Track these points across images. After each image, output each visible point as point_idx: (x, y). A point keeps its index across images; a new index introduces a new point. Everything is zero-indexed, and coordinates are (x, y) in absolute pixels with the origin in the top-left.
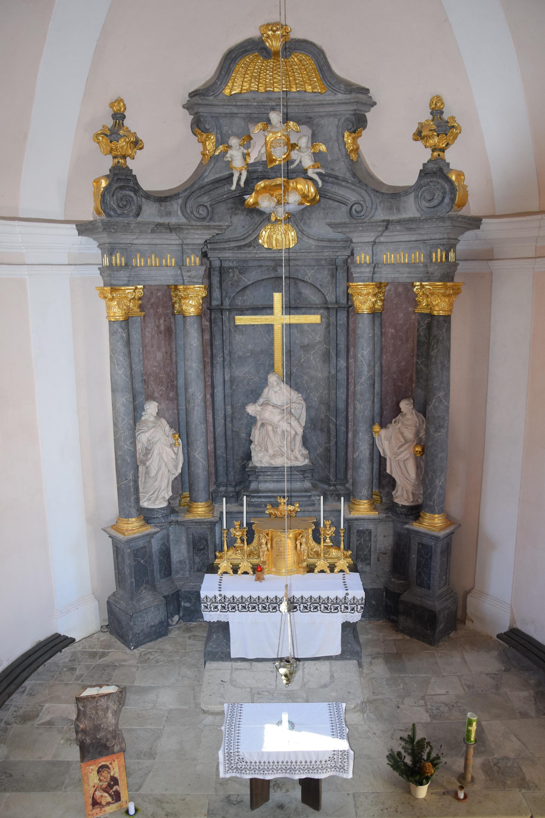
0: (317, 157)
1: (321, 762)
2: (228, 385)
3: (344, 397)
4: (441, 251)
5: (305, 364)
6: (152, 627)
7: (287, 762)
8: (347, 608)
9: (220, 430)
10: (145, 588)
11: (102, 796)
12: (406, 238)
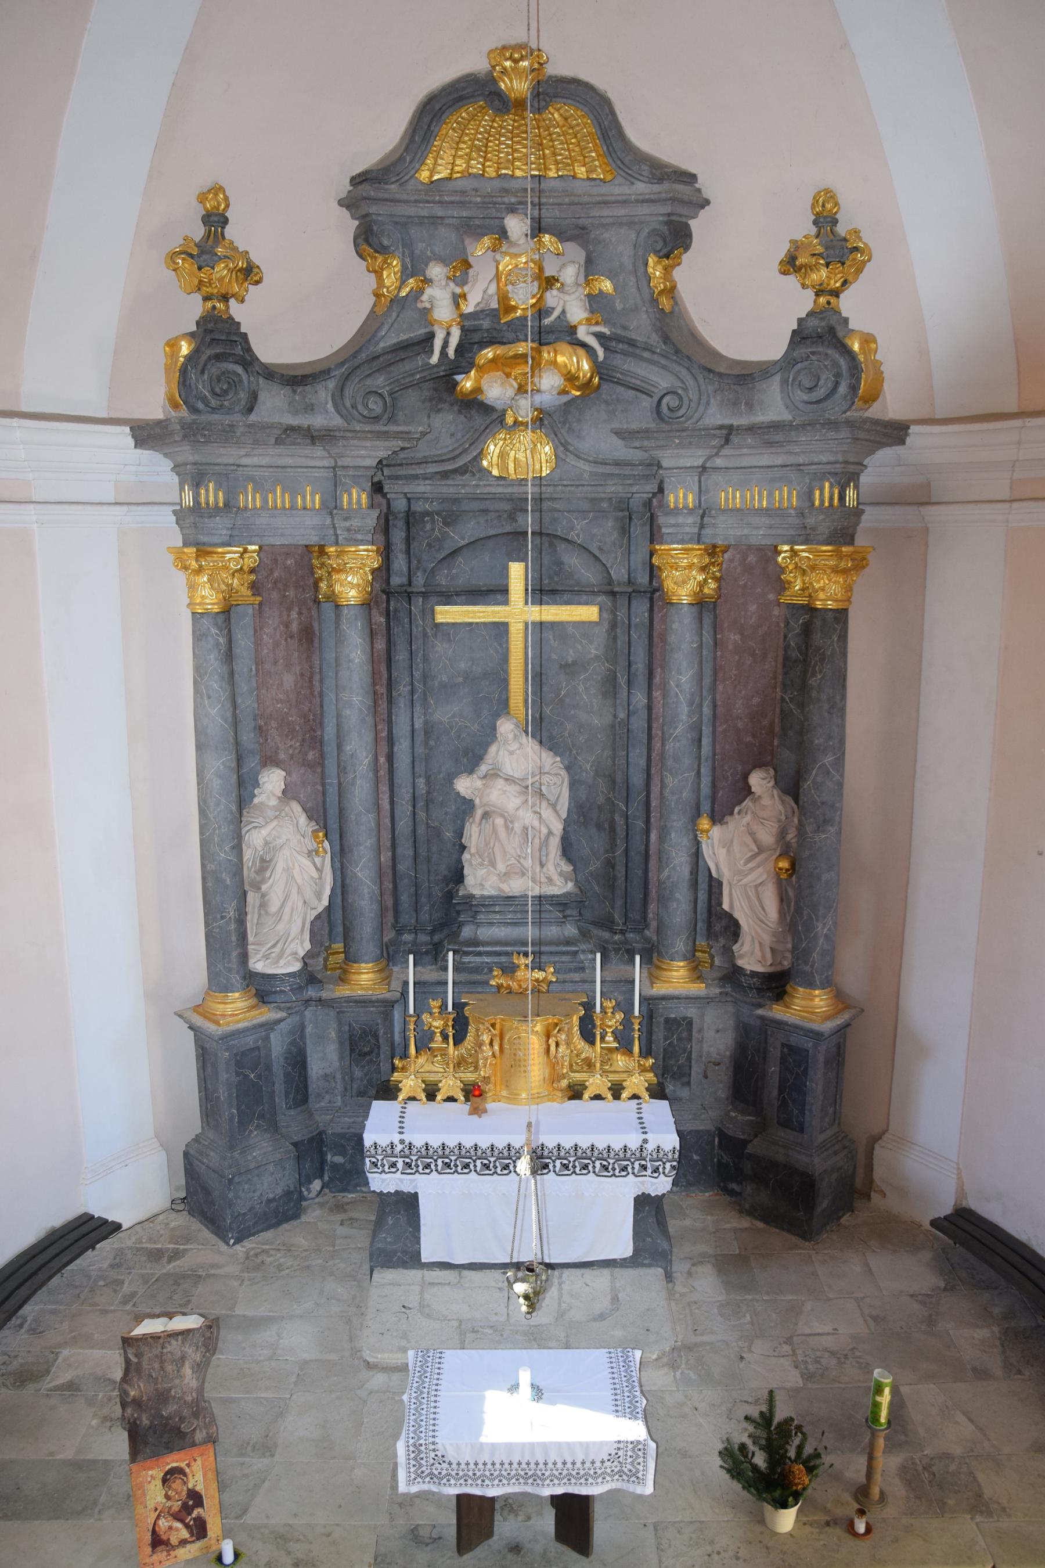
0: (595, 302)
1: (593, 1463)
2: (420, 738)
3: (643, 762)
4: (831, 487)
6: (269, 1201)
7: (528, 1464)
8: (644, 1168)
9: (403, 824)
10: (258, 1127)
11: (170, 1528)
12: (765, 460)
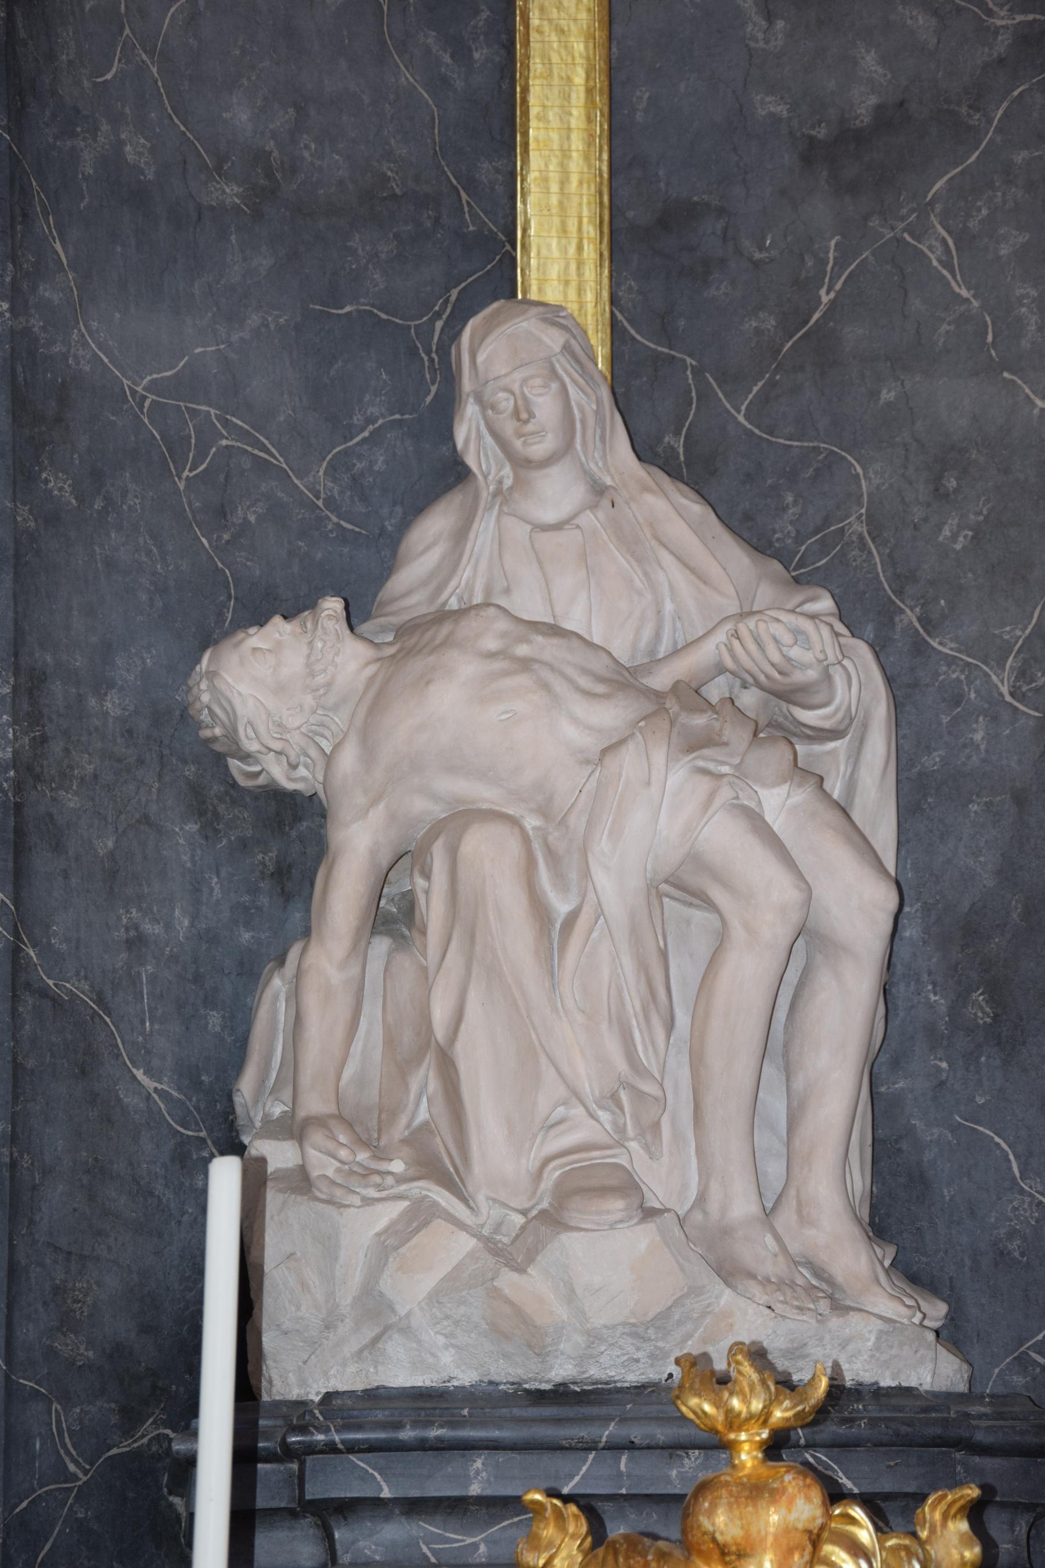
5: (854, 334)
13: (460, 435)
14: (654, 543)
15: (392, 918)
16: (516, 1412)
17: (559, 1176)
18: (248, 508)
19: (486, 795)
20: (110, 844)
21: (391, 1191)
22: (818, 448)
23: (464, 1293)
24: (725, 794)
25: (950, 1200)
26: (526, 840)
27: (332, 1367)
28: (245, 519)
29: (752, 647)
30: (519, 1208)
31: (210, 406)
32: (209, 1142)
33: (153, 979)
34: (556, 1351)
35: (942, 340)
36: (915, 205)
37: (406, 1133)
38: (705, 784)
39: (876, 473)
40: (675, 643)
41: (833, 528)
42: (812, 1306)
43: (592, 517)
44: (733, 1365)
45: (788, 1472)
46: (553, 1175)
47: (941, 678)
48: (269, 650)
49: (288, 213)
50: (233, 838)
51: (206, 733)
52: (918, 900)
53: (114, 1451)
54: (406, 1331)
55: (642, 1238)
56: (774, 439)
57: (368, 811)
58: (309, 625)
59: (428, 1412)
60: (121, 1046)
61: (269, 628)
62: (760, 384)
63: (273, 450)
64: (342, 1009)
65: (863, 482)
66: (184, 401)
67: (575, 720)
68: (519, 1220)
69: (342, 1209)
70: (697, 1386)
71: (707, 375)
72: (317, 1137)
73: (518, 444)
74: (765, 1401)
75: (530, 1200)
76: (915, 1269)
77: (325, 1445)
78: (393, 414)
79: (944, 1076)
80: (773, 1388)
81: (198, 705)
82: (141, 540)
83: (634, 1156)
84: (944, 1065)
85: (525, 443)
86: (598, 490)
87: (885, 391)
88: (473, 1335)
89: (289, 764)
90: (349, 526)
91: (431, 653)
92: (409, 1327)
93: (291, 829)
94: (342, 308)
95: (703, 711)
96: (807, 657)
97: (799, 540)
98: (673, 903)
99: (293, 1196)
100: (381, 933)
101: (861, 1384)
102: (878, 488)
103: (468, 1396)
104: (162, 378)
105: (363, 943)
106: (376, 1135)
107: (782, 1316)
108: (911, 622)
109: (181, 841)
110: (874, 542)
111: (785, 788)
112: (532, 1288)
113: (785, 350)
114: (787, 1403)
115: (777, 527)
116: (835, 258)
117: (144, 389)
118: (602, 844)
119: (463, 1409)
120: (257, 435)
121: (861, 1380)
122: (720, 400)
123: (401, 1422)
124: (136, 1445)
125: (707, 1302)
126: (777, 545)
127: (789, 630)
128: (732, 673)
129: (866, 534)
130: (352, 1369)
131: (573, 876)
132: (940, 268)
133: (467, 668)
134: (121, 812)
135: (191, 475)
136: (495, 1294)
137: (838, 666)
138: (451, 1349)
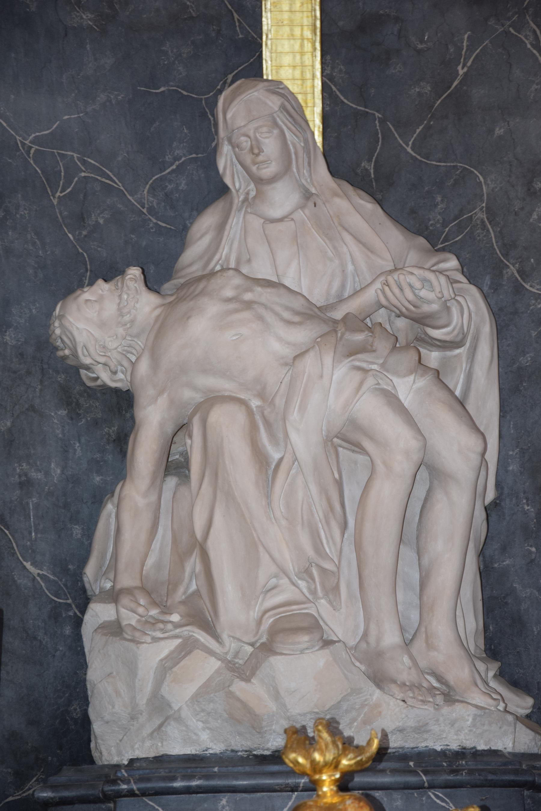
13: (221, 164)
14: (340, 228)
15: (174, 466)
16: (248, 769)
17: (272, 622)
18: (99, 215)
19: (226, 386)
20: (9, 424)
21: (170, 633)
22: (457, 166)
23: (212, 695)
24: (370, 382)
25: (538, 634)
26: (250, 412)
27: (136, 743)
28: (97, 221)
29: (397, 291)
30: (248, 642)
31: (74, 152)
32: (73, 606)
33: (37, 506)
34: (270, 730)
35: (533, 95)
36: (517, 10)
37: (183, 597)
38: (357, 376)
39: (492, 181)
40: (355, 289)
41: (465, 216)
42: (431, 700)
43: (302, 213)
44: (316, 732)
45: (349, 798)
46: (268, 622)
47: (531, 308)
48: (95, 301)
49: (123, 30)
50: (89, 419)
51: (60, 353)
52: (517, 447)
53: (10, 799)
54: (178, 719)
55: (320, 659)
56: (429, 162)
57: (157, 398)
58: (119, 284)
59: (192, 770)
60: (16, 548)
61: (95, 287)
62: (421, 127)
63: (115, 179)
64: (146, 521)
65: (484, 186)
66: (56, 149)
67: (280, 339)
68: (250, 649)
69: (139, 645)
70: (295, 746)
71: (388, 123)
72: (125, 600)
73: (254, 168)
74: (334, 754)
75: (255, 636)
76: (516, 677)
77: (128, 791)
78: (191, 154)
79: (533, 556)
80: (340, 746)
81: (54, 336)
82: (29, 236)
83: (323, 608)
84: (533, 549)
85: (258, 168)
86: (307, 196)
87: (497, 129)
88: (219, 721)
89: (111, 371)
90: (164, 225)
91: (192, 299)
92: (180, 717)
93: (126, 412)
94: (158, 89)
95: (362, 331)
96: (431, 296)
97: (445, 224)
98: (345, 451)
99: (111, 637)
100: (171, 474)
101: (465, 748)
102: (493, 190)
103: (219, 759)
104: (42, 135)
105: (158, 482)
106: (165, 599)
107: (411, 706)
108: (514, 274)
109: (56, 421)
110: (490, 224)
111: (412, 377)
112: (252, 692)
113: (436, 105)
114: (351, 756)
115: (431, 217)
116: (467, 46)
117: (30, 142)
118: (294, 415)
119: (214, 767)
120: (104, 169)
121: (465, 745)
122: (396, 138)
123: (174, 776)
124: (24, 795)
125: (364, 698)
126: (431, 228)
127: (419, 279)
128: (386, 308)
129: (486, 220)
130: (148, 744)
131: (281, 435)
132: (532, 49)
133: (212, 308)
134: (16, 404)
135: (61, 195)
136: (231, 695)
137: (453, 301)
138: (207, 730)
